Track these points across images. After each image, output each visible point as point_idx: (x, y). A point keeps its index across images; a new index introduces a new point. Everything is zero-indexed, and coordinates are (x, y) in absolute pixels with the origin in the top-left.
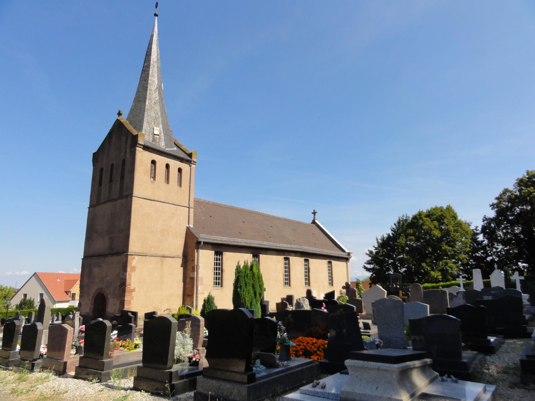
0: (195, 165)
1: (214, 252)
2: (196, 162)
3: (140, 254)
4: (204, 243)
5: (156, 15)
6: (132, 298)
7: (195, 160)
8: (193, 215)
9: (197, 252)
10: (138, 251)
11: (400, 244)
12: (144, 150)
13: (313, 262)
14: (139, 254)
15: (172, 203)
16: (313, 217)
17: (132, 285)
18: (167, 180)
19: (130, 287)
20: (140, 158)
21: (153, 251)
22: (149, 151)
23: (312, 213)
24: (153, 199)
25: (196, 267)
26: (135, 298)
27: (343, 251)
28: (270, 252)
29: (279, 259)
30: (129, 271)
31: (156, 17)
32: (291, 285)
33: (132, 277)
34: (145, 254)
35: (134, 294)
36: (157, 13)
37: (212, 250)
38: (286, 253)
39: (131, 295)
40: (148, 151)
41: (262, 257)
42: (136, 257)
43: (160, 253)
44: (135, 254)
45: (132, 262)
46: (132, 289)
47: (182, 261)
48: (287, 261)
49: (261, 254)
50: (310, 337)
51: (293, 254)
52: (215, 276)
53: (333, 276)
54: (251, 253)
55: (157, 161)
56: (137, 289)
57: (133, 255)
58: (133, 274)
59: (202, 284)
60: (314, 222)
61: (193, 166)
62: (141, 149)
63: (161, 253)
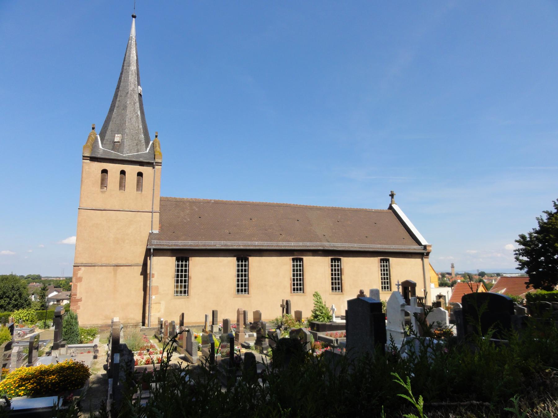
0: (161, 165)
1: (174, 258)
2: (161, 163)
3: (87, 265)
4: (154, 249)
5: (134, 17)
6: (79, 308)
7: (159, 161)
8: (159, 220)
9: (150, 259)
10: (85, 262)
11: (553, 225)
12: (91, 162)
13: (308, 260)
14: (85, 265)
15: (128, 210)
16: (391, 200)
17: (78, 295)
18: (122, 185)
19: (76, 297)
20: (87, 170)
21: (104, 261)
22: (98, 161)
23: (390, 195)
24: (103, 209)
25: (149, 275)
26: (81, 308)
27: (419, 243)
28: (308, 253)
29: (326, 261)
30: (75, 282)
31: (134, 18)
32: (304, 292)
33: (78, 287)
34: (93, 265)
35: (80, 304)
36: (134, 15)
37: (172, 256)
38: (295, 253)
39: (77, 304)
40: (97, 162)
41: (253, 261)
42: (83, 268)
43: (114, 263)
44: (81, 265)
45: (77, 273)
46: (78, 299)
47: (142, 269)
48: (384, 263)
49: (251, 256)
50: (11, 346)
51: (311, 254)
52: (383, 285)
53: (391, 278)
54: (234, 256)
55: (108, 170)
56: (83, 299)
57: (79, 266)
58: (79, 284)
59: (157, 294)
60: (391, 208)
61: (157, 167)
62: (89, 161)
63: (114, 263)
